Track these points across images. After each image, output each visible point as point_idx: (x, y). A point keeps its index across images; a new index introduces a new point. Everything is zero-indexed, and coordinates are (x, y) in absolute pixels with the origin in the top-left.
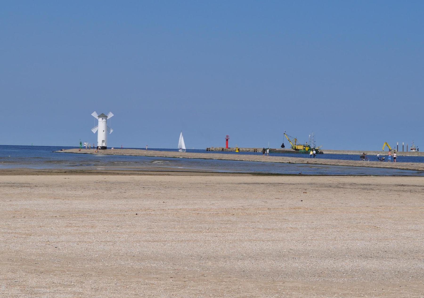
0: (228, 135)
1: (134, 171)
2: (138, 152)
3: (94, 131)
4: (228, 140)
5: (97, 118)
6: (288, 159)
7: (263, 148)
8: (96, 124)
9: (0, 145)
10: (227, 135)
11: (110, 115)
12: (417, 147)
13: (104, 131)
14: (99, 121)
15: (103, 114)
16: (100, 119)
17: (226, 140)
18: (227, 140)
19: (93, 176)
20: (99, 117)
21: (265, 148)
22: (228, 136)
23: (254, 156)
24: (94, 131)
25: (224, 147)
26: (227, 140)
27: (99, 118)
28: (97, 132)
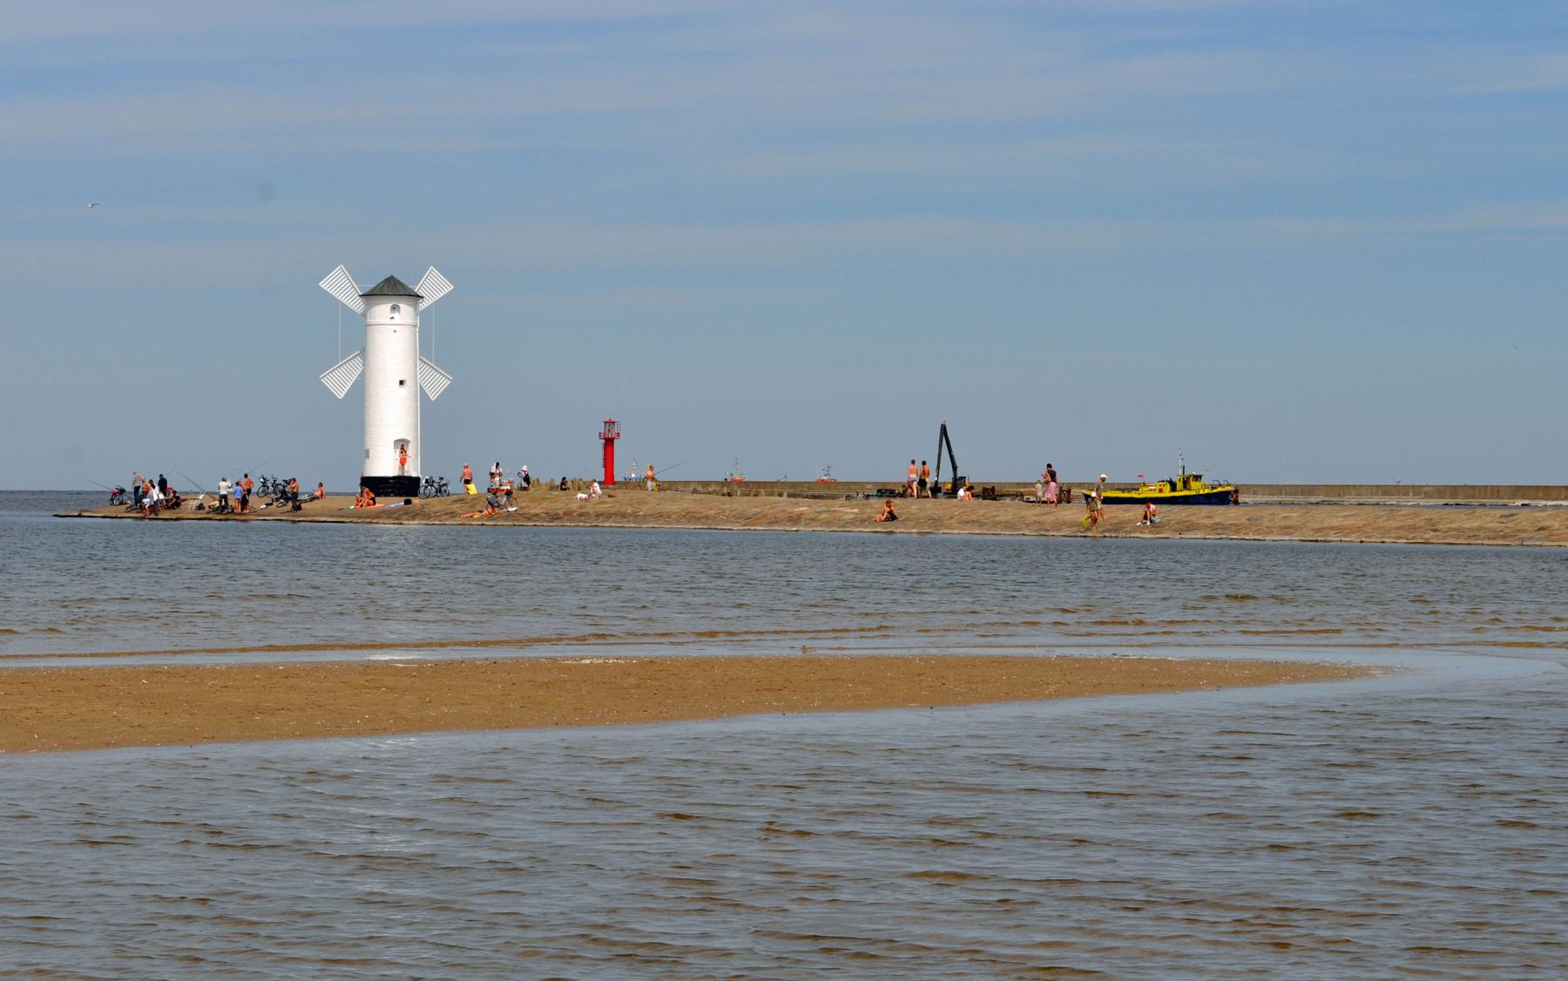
3: (338, 382)
5: (356, 304)
8: (356, 340)
10: (607, 420)
11: (434, 287)
13: (401, 383)
17: (604, 441)
18: (609, 443)
20: (371, 296)
22: (614, 423)
26: (609, 443)
28: (360, 391)
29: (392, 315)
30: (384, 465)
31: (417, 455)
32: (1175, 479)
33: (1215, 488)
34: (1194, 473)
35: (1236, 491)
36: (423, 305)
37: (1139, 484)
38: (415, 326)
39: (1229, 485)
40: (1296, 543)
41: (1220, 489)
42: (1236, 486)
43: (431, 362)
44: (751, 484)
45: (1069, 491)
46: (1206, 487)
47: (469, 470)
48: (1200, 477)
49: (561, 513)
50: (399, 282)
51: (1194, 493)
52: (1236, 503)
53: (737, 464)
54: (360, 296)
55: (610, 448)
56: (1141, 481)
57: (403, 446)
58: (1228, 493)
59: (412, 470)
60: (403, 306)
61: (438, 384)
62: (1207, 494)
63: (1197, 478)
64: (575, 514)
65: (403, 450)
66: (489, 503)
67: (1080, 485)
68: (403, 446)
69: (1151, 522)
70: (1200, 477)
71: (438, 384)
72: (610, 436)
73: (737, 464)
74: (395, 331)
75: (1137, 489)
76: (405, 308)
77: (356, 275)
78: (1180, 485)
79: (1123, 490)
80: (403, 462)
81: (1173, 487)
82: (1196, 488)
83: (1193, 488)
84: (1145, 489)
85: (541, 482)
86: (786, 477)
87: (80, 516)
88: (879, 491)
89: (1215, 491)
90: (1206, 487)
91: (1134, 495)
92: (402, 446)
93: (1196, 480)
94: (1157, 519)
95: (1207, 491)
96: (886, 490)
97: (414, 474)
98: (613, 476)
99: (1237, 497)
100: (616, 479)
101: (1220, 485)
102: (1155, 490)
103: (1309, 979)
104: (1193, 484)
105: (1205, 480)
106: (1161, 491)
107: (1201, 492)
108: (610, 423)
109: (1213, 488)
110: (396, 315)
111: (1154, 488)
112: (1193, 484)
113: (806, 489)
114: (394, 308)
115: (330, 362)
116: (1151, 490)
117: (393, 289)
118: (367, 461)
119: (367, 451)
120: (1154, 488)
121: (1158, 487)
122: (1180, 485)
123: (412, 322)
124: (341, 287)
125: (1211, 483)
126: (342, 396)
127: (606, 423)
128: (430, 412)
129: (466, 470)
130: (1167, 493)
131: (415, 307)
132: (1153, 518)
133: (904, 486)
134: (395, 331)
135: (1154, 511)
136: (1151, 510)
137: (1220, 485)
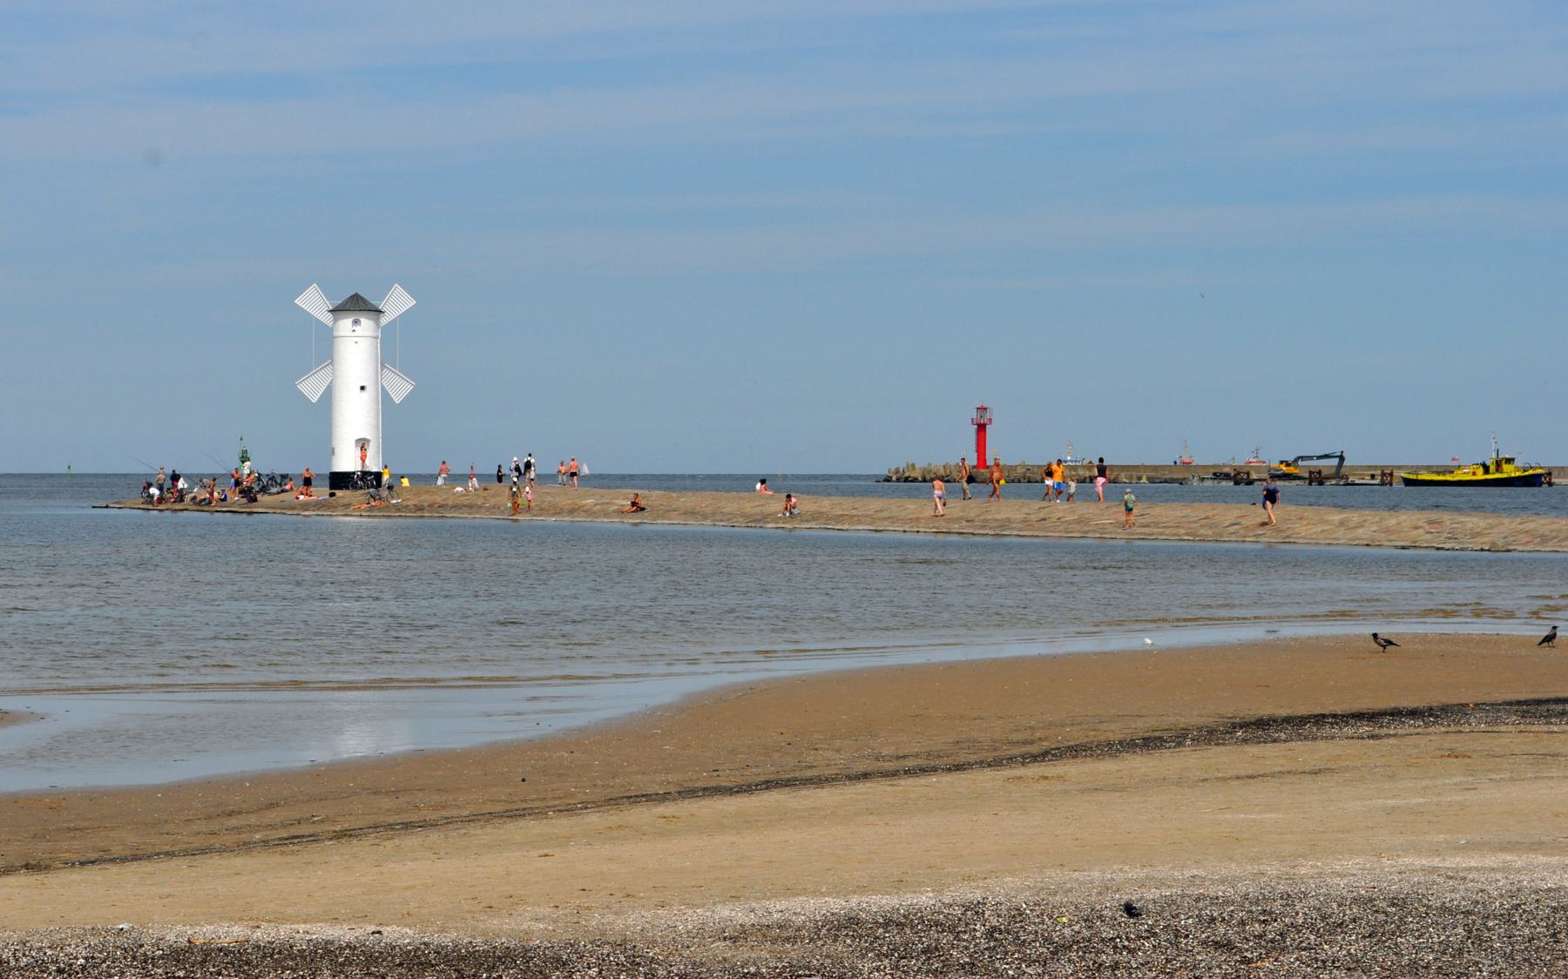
0: (985, 406)
1: (1245, 619)
2: (549, 498)
3: (312, 388)
4: (988, 427)
5: (327, 319)
6: (1470, 525)
7: (171, 472)
8: (323, 350)
9: (2, 472)
10: (979, 406)
11: (397, 303)
12: (573, 460)
13: (363, 388)
14: (336, 333)
15: (356, 295)
16: (345, 324)
17: (976, 427)
18: (981, 428)
19: (979, 658)
20: (337, 311)
21: (177, 472)
22: (986, 409)
23: (1243, 512)
24: (312, 388)
25: (972, 460)
26: (981, 428)
27: (335, 321)
28: (328, 396)
29: (354, 328)
30: (347, 462)
31: (378, 453)
32: (1488, 463)
33: (1527, 471)
34: (1507, 456)
35: (1549, 474)
36: (385, 320)
37: (1453, 466)
38: (377, 338)
39: (1541, 468)
40: (863, 534)
41: (1531, 472)
42: (1550, 468)
43: (395, 367)
44: (1115, 468)
45: (1391, 474)
46: (1518, 469)
47: (575, 463)
48: (1513, 460)
49: (426, 504)
50: (362, 298)
51: (1505, 476)
52: (1550, 484)
53: (1186, 447)
54: (329, 311)
55: (982, 433)
56: (1456, 463)
57: (364, 444)
58: (1540, 475)
59: (373, 466)
60: (363, 320)
61: (400, 389)
62: (1519, 477)
63: (1509, 461)
64: (436, 506)
65: (363, 448)
66: (371, 496)
67: (1400, 468)
68: (364, 444)
69: (791, 513)
70: (1513, 460)
71: (400, 389)
72: (982, 422)
73: (1186, 447)
74: (356, 342)
75: (1453, 472)
76: (367, 324)
77: (325, 290)
78: (1492, 468)
79: (1438, 473)
80: (363, 459)
81: (1486, 469)
82: (1509, 471)
83: (1505, 471)
84: (1459, 472)
85: (916, 466)
86: (1234, 459)
87: (107, 507)
88: (1215, 474)
89: (1526, 473)
90: (1518, 469)
91: (1449, 478)
92: (363, 444)
93: (1509, 463)
94: (796, 511)
95: (1518, 474)
96: (1221, 474)
97: (374, 469)
98: (985, 460)
99: (1550, 479)
100: (988, 464)
101: (1531, 468)
102: (1469, 473)
103: (762, 957)
104: (1506, 467)
105: (1518, 463)
106: (1474, 474)
107: (1513, 475)
108: (982, 409)
109: (1525, 471)
110: (357, 328)
111: (1467, 470)
112: (1506, 467)
113: (1167, 473)
114: (356, 322)
115: (305, 370)
116: (1465, 473)
117: (356, 305)
118: (334, 458)
119: (334, 449)
120: (1467, 470)
121: (1471, 470)
122: (1492, 468)
123: (374, 334)
124: (314, 302)
125: (1523, 465)
126: (316, 400)
127: (978, 409)
128: (388, 410)
129: (572, 463)
130: (1480, 476)
131: (377, 322)
132: (792, 510)
133: (1235, 470)
134: (356, 342)
135: (795, 503)
136: (792, 503)
137: (1531, 468)
